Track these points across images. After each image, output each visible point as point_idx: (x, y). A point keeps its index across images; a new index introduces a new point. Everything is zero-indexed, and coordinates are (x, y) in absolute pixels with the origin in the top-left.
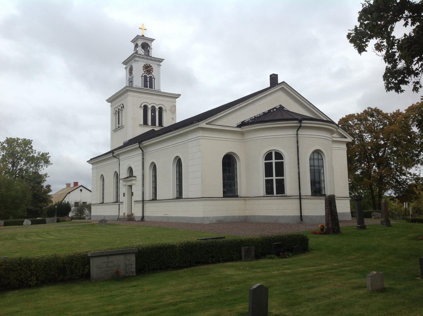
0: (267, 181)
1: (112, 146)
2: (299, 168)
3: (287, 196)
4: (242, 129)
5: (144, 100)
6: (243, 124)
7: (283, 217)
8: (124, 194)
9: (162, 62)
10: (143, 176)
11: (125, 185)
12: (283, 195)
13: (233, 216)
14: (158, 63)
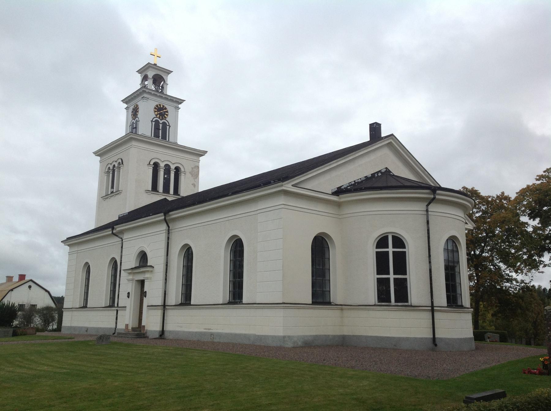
0: (379, 281)
1: (97, 220)
2: (430, 262)
3: (411, 306)
4: (340, 198)
5: (155, 155)
6: (339, 192)
7: (407, 339)
8: (129, 293)
9: (181, 103)
10: (167, 265)
11: (132, 280)
12: (406, 304)
13: (325, 335)
14: (175, 105)
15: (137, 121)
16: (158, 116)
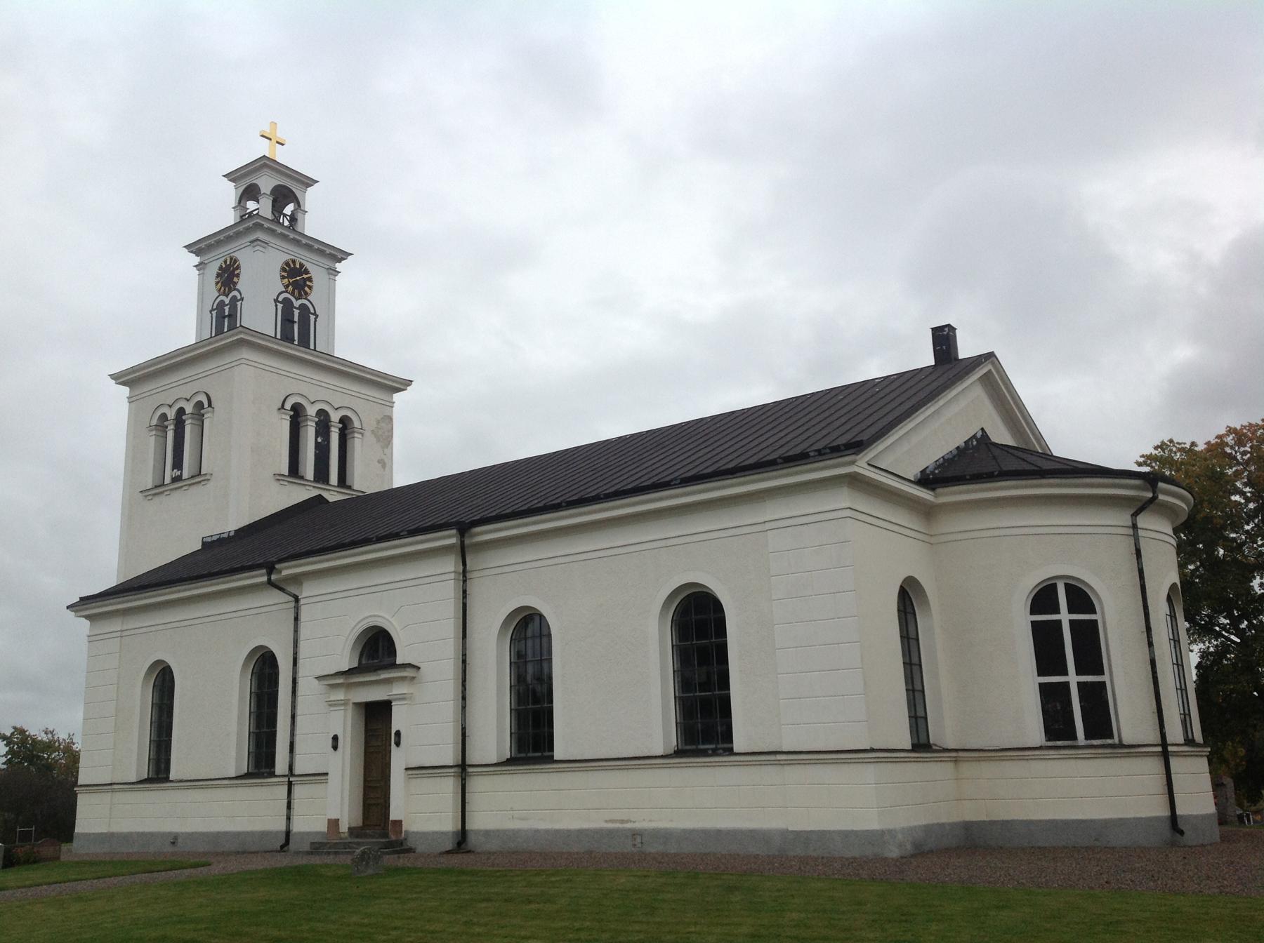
3: (1121, 745)
4: (936, 497)
7: (1121, 822)
8: (335, 738)
9: (340, 261)
10: (464, 661)
11: (345, 703)
12: (1109, 741)
14: (328, 263)
15: (234, 299)
16: (290, 288)
